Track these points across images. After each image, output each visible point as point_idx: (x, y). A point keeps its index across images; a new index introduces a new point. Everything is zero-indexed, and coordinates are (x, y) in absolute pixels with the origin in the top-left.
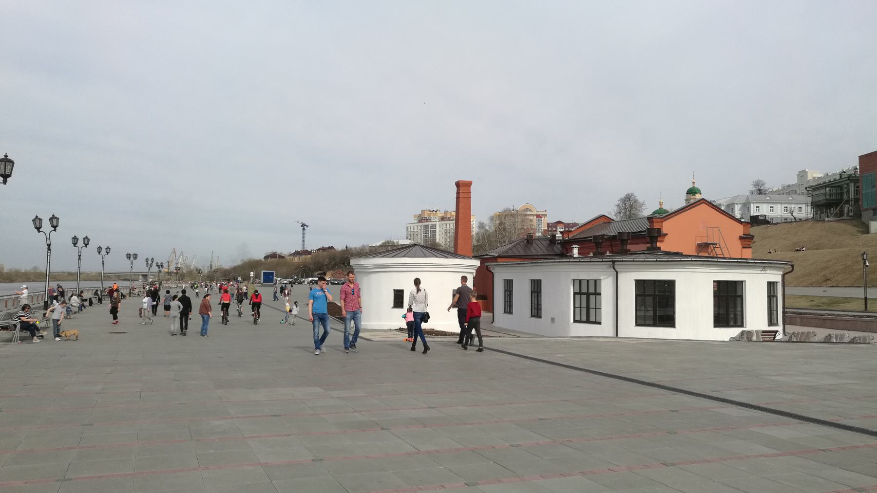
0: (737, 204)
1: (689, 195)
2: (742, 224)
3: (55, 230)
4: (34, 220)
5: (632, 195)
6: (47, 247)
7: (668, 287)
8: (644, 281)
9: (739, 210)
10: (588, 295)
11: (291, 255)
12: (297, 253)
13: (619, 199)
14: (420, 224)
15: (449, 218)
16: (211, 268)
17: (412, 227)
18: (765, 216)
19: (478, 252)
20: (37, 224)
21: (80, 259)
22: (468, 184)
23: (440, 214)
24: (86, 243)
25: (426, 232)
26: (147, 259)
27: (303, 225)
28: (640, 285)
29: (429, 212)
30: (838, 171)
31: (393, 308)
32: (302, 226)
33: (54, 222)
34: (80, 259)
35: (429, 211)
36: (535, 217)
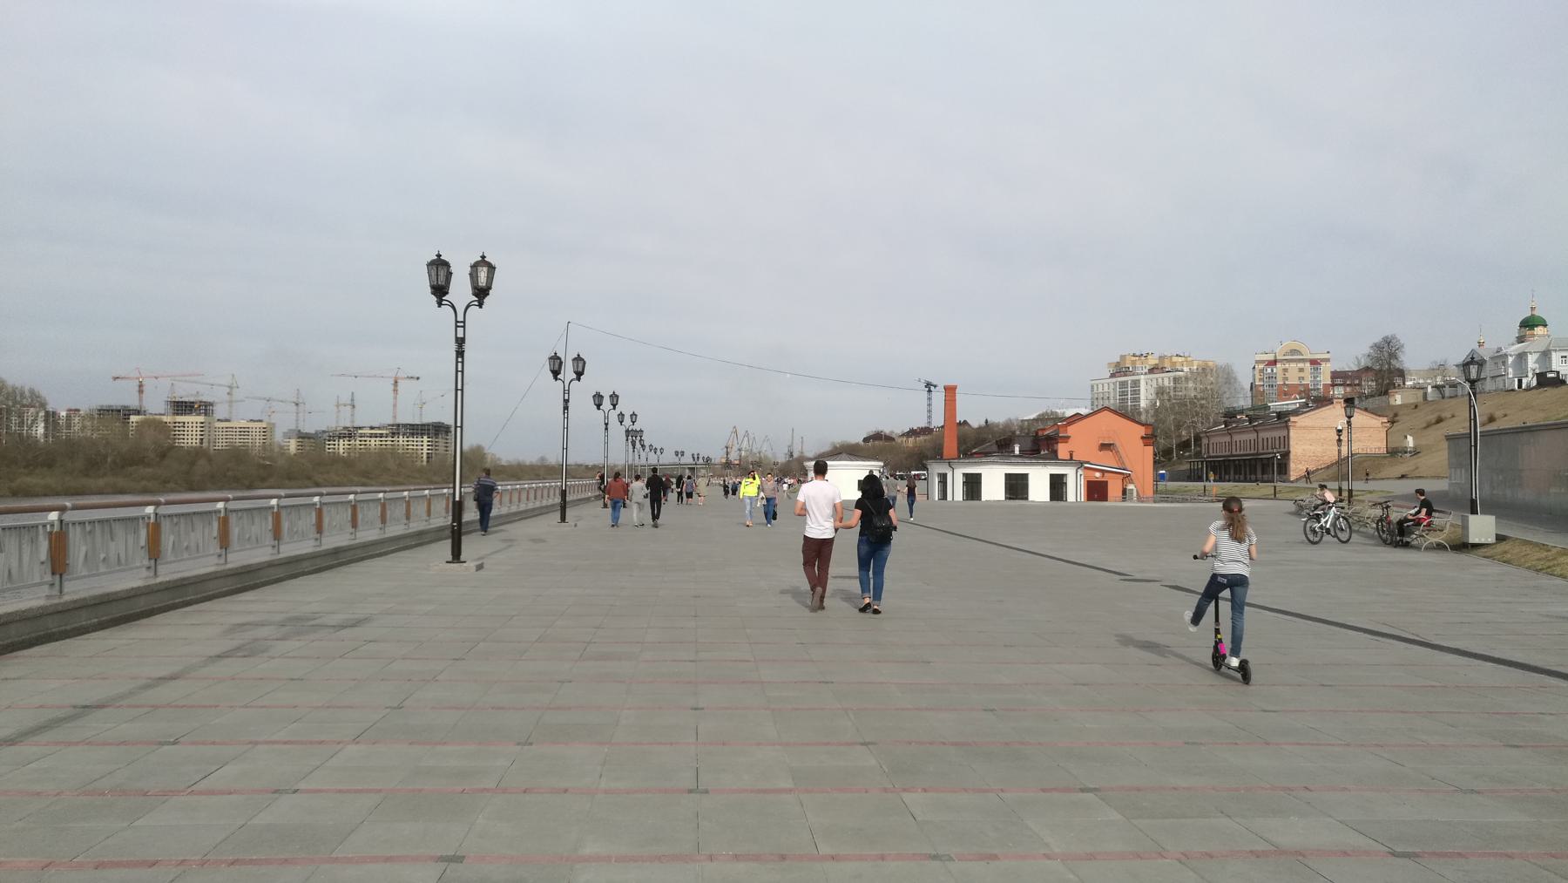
0: (1531, 353)
1: (1523, 329)
3: (579, 379)
5: (1394, 337)
7: (1025, 477)
9: (1535, 363)
11: (903, 435)
12: (912, 433)
13: (1371, 344)
14: (1114, 380)
15: (1162, 368)
16: (791, 455)
17: (1100, 386)
18: (1558, 373)
21: (606, 429)
23: (1153, 361)
24: (556, 368)
25: (1123, 394)
26: (693, 455)
27: (928, 384)
28: (966, 475)
29: (1134, 358)
32: (926, 387)
33: (614, 398)
34: (606, 429)
35: (1134, 355)
36: (1308, 364)
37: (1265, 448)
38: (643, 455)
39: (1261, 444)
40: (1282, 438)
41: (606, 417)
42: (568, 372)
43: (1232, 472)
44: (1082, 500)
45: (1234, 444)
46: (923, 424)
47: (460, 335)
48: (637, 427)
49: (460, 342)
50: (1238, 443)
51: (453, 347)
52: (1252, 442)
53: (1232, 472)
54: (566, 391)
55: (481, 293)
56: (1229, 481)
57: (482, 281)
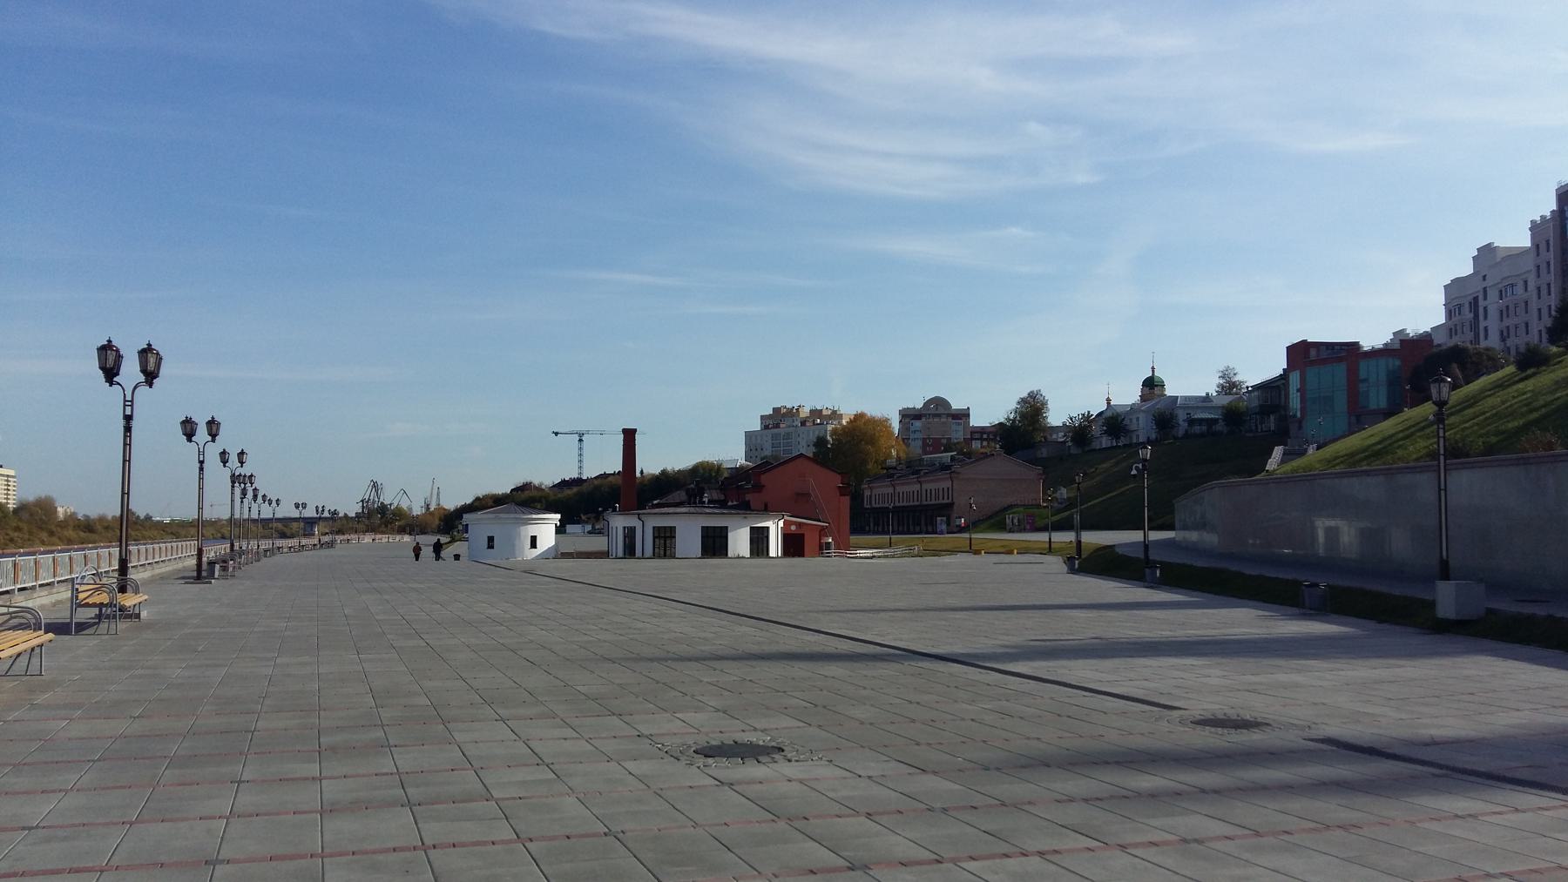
3: (213, 441)
4: (183, 423)
6: (198, 465)
7: (672, 529)
8: (707, 527)
19: (1118, 438)
20: (189, 428)
22: (634, 431)
30: (1013, 405)
33: (213, 427)
38: (255, 507)
40: (946, 490)
41: (201, 453)
42: (130, 371)
43: (923, 522)
44: (780, 555)
46: (575, 476)
47: (128, 412)
48: (246, 470)
49: (128, 419)
51: (122, 423)
53: (923, 522)
54: (129, 403)
55: (150, 376)
57: (151, 366)
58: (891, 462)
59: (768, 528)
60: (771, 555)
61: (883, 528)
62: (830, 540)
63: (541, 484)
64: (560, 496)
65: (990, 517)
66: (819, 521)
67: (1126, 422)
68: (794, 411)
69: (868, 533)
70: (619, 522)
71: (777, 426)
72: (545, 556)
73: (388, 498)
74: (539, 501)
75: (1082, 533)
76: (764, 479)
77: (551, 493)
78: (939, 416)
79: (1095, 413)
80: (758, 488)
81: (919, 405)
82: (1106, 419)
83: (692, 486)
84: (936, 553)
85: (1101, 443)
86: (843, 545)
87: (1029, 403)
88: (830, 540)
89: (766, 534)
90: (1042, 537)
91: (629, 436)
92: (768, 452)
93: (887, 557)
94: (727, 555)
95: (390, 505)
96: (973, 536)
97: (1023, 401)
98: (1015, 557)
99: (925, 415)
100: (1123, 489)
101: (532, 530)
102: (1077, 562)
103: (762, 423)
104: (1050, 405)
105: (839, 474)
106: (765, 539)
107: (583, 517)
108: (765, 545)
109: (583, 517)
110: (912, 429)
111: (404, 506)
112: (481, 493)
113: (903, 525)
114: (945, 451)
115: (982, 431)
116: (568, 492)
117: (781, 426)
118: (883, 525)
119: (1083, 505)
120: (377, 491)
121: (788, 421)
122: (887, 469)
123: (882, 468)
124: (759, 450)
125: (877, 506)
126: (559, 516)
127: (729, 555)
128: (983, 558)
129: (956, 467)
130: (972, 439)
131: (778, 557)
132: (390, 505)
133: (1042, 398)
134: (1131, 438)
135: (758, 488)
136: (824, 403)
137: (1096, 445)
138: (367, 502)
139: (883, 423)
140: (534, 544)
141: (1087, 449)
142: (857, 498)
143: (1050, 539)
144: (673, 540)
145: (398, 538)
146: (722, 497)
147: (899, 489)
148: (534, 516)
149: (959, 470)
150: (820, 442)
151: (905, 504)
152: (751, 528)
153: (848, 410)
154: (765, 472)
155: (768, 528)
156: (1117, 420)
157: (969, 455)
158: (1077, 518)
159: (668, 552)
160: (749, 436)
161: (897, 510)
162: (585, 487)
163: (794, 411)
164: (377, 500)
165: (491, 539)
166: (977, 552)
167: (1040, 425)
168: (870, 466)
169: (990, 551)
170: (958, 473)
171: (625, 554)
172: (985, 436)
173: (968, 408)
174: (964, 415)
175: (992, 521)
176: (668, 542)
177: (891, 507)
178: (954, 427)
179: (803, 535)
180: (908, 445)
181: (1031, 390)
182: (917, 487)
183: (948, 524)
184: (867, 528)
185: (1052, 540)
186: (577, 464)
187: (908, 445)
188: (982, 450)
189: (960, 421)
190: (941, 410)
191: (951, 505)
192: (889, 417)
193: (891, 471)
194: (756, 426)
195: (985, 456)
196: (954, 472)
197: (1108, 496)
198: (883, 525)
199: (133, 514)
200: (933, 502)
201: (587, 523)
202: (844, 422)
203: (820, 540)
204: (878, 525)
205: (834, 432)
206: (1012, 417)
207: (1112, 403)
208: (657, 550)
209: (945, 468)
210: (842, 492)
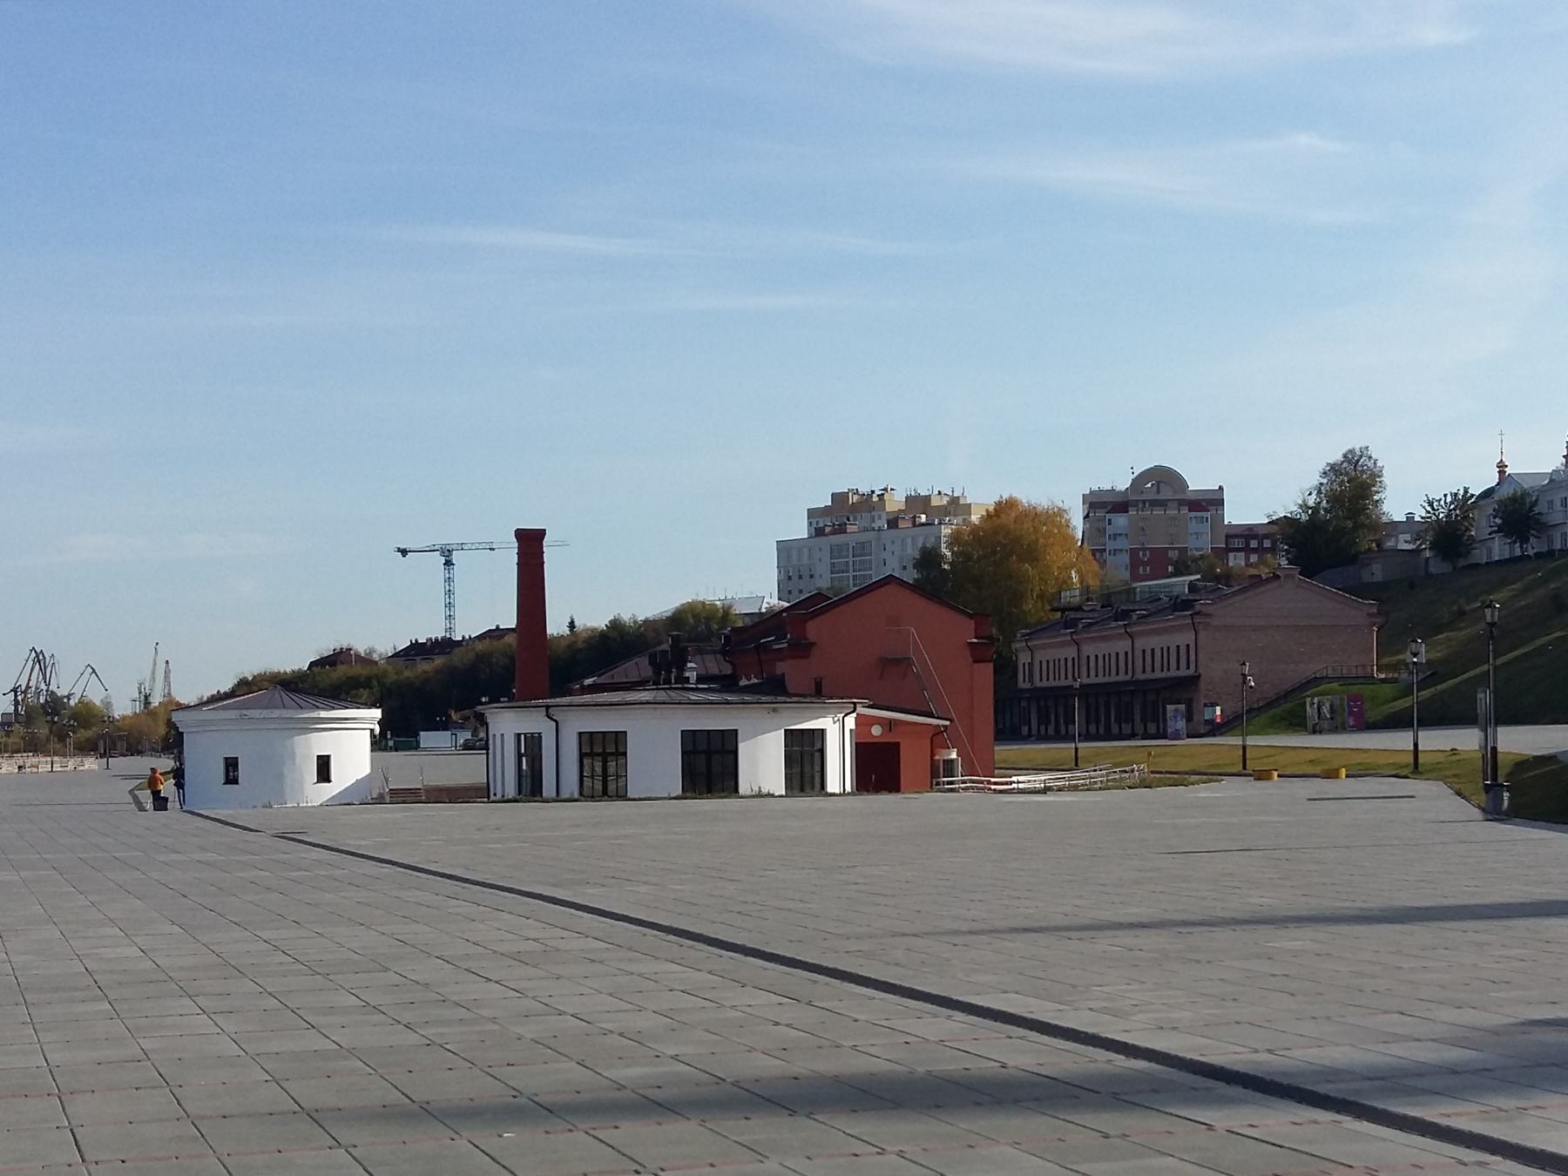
2: (971, 618)
7: (619, 738)
10: (605, 757)
22: (541, 534)
30: (1315, 479)
31: (224, 784)
37: (1148, 668)
39: (1139, 662)
43: (1137, 718)
44: (848, 789)
45: (1084, 661)
46: (438, 633)
50: (1092, 659)
52: (1122, 657)
53: (1137, 718)
56: (1132, 736)
58: (1072, 596)
59: (823, 731)
60: (830, 789)
61: (1108, 728)
62: (954, 756)
63: (372, 651)
64: (407, 673)
65: (1270, 705)
66: (932, 716)
67: (1542, 507)
68: (875, 499)
69: (1027, 739)
70: (507, 724)
71: (841, 529)
72: (344, 800)
73: (65, 683)
74: (366, 683)
75: (1499, 729)
76: (813, 630)
77: (390, 668)
78: (1162, 504)
79: (1476, 490)
80: (802, 649)
81: (1123, 483)
82: (1500, 502)
83: (665, 647)
84: (1178, 778)
85: (1490, 551)
86: (981, 766)
87: (1347, 474)
88: (954, 756)
89: (818, 746)
90: (1400, 741)
91: (530, 544)
92: (823, 582)
93: (1075, 788)
94: (736, 790)
95: (68, 697)
96: (1252, 741)
97: (1334, 470)
98: (1343, 785)
99: (1135, 504)
100: (1538, 642)
101: (321, 743)
102: (1506, 795)
103: (810, 524)
104: (1387, 478)
105: (970, 616)
106: (817, 755)
107: (454, 716)
108: (817, 768)
109: (454, 716)
110: (1110, 530)
111: (96, 697)
112: (250, 670)
113: (1097, 722)
114: (1177, 573)
115: (1248, 534)
116: (424, 667)
117: (850, 528)
118: (1057, 722)
119: (1482, 674)
120: (43, 671)
121: (863, 520)
122: (1063, 610)
123: (1054, 610)
124: (806, 577)
125: (1045, 684)
126: (377, 713)
127: (742, 791)
128: (1275, 788)
129: (1203, 603)
130: (1228, 550)
131: (844, 794)
132: (68, 697)
133: (1370, 464)
134: (1550, 540)
135: (802, 649)
136: (933, 482)
137: (1479, 556)
138: (25, 692)
139: (1053, 519)
140: (324, 769)
141: (1462, 563)
142: (1005, 669)
143: (1416, 745)
144: (621, 761)
145: (71, 763)
146: (728, 670)
147: (1089, 650)
148: (323, 714)
149: (1210, 610)
150: (929, 559)
151: (1100, 680)
152: (785, 730)
153: (981, 498)
154: (815, 615)
155: (823, 731)
156: (1524, 504)
157: (1227, 578)
158: (1484, 699)
159: (612, 787)
160: (785, 548)
161: (1087, 691)
162: (457, 657)
163: (875, 499)
164: (43, 687)
165: (231, 764)
166: (1263, 775)
167: (1369, 517)
168: (1029, 605)
169: (1288, 772)
170: (1209, 615)
171: (520, 793)
172: (1254, 544)
173: (1221, 488)
174: (1212, 502)
175: (1277, 711)
176: (612, 765)
177: (1077, 685)
178: (1193, 527)
179: (897, 745)
180: (1103, 564)
181: (1350, 447)
182: (1123, 645)
183: (1189, 717)
184: (1025, 730)
185: (1420, 748)
186: (441, 612)
187: (1103, 564)
188: (1252, 571)
189: (1204, 514)
190: (1166, 494)
191: (1194, 680)
192: (1066, 508)
193: (1072, 615)
194: (799, 530)
195: (1257, 581)
196: (1199, 613)
197: (1515, 653)
198: (1057, 722)
199: (1482, 730)
200: (1158, 675)
201: (462, 727)
202: (975, 518)
203: (933, 755)
204: (1047, 724)
205: (955, 539)
206: (1311, 501)
207: (1508, 471)
208: (587, 782)
209: (1180, 605)
210: (978, 654)
